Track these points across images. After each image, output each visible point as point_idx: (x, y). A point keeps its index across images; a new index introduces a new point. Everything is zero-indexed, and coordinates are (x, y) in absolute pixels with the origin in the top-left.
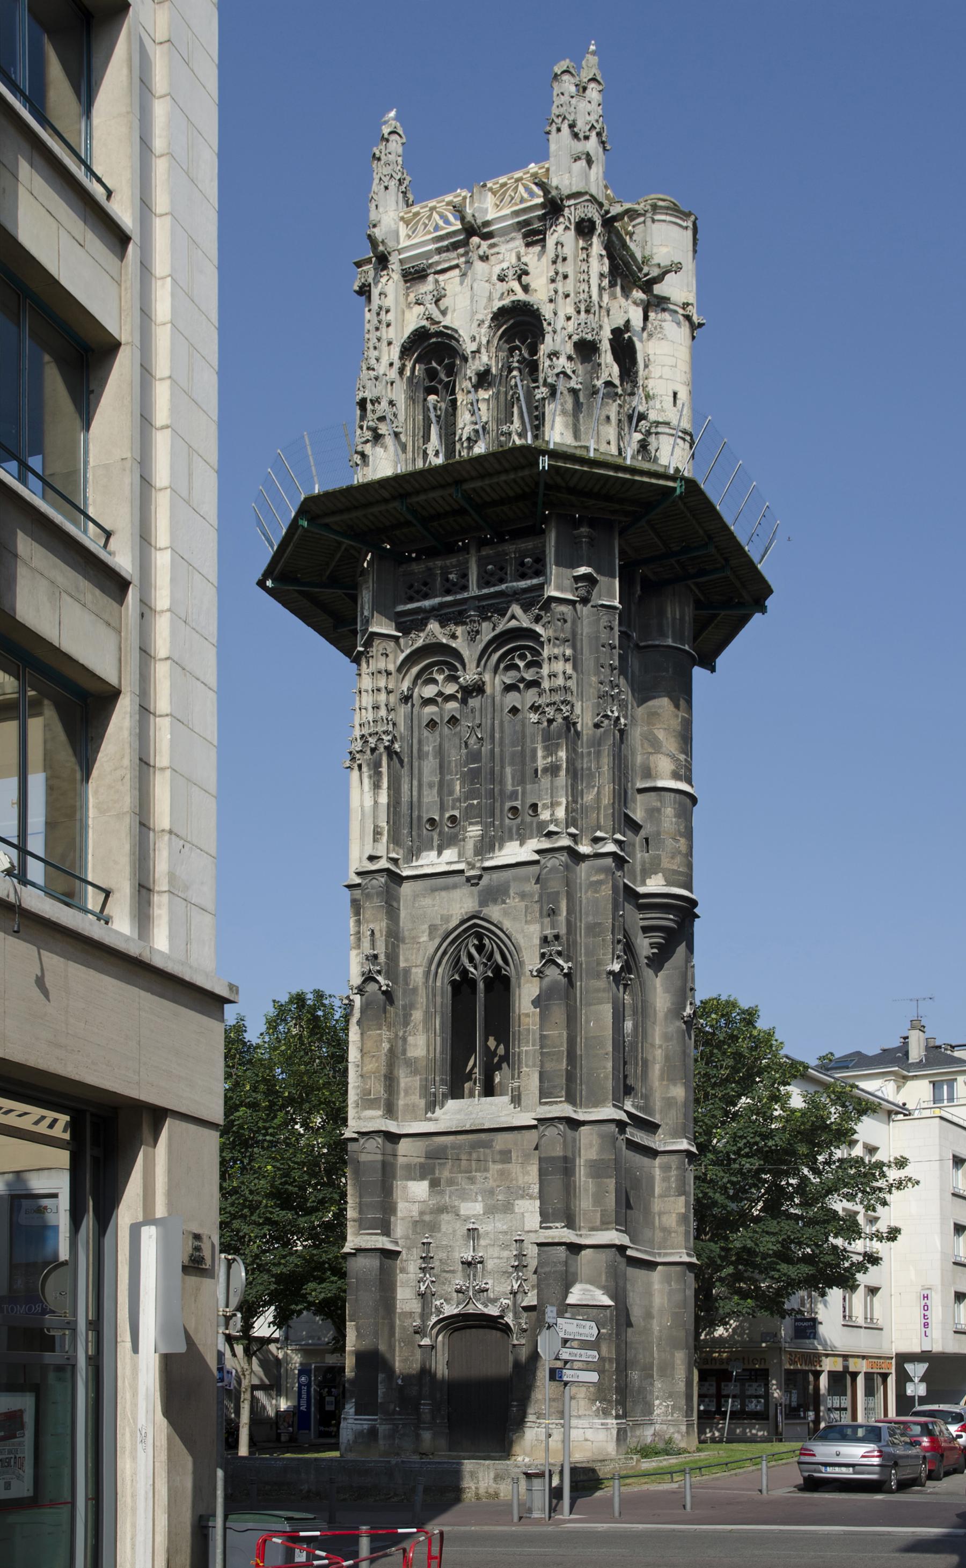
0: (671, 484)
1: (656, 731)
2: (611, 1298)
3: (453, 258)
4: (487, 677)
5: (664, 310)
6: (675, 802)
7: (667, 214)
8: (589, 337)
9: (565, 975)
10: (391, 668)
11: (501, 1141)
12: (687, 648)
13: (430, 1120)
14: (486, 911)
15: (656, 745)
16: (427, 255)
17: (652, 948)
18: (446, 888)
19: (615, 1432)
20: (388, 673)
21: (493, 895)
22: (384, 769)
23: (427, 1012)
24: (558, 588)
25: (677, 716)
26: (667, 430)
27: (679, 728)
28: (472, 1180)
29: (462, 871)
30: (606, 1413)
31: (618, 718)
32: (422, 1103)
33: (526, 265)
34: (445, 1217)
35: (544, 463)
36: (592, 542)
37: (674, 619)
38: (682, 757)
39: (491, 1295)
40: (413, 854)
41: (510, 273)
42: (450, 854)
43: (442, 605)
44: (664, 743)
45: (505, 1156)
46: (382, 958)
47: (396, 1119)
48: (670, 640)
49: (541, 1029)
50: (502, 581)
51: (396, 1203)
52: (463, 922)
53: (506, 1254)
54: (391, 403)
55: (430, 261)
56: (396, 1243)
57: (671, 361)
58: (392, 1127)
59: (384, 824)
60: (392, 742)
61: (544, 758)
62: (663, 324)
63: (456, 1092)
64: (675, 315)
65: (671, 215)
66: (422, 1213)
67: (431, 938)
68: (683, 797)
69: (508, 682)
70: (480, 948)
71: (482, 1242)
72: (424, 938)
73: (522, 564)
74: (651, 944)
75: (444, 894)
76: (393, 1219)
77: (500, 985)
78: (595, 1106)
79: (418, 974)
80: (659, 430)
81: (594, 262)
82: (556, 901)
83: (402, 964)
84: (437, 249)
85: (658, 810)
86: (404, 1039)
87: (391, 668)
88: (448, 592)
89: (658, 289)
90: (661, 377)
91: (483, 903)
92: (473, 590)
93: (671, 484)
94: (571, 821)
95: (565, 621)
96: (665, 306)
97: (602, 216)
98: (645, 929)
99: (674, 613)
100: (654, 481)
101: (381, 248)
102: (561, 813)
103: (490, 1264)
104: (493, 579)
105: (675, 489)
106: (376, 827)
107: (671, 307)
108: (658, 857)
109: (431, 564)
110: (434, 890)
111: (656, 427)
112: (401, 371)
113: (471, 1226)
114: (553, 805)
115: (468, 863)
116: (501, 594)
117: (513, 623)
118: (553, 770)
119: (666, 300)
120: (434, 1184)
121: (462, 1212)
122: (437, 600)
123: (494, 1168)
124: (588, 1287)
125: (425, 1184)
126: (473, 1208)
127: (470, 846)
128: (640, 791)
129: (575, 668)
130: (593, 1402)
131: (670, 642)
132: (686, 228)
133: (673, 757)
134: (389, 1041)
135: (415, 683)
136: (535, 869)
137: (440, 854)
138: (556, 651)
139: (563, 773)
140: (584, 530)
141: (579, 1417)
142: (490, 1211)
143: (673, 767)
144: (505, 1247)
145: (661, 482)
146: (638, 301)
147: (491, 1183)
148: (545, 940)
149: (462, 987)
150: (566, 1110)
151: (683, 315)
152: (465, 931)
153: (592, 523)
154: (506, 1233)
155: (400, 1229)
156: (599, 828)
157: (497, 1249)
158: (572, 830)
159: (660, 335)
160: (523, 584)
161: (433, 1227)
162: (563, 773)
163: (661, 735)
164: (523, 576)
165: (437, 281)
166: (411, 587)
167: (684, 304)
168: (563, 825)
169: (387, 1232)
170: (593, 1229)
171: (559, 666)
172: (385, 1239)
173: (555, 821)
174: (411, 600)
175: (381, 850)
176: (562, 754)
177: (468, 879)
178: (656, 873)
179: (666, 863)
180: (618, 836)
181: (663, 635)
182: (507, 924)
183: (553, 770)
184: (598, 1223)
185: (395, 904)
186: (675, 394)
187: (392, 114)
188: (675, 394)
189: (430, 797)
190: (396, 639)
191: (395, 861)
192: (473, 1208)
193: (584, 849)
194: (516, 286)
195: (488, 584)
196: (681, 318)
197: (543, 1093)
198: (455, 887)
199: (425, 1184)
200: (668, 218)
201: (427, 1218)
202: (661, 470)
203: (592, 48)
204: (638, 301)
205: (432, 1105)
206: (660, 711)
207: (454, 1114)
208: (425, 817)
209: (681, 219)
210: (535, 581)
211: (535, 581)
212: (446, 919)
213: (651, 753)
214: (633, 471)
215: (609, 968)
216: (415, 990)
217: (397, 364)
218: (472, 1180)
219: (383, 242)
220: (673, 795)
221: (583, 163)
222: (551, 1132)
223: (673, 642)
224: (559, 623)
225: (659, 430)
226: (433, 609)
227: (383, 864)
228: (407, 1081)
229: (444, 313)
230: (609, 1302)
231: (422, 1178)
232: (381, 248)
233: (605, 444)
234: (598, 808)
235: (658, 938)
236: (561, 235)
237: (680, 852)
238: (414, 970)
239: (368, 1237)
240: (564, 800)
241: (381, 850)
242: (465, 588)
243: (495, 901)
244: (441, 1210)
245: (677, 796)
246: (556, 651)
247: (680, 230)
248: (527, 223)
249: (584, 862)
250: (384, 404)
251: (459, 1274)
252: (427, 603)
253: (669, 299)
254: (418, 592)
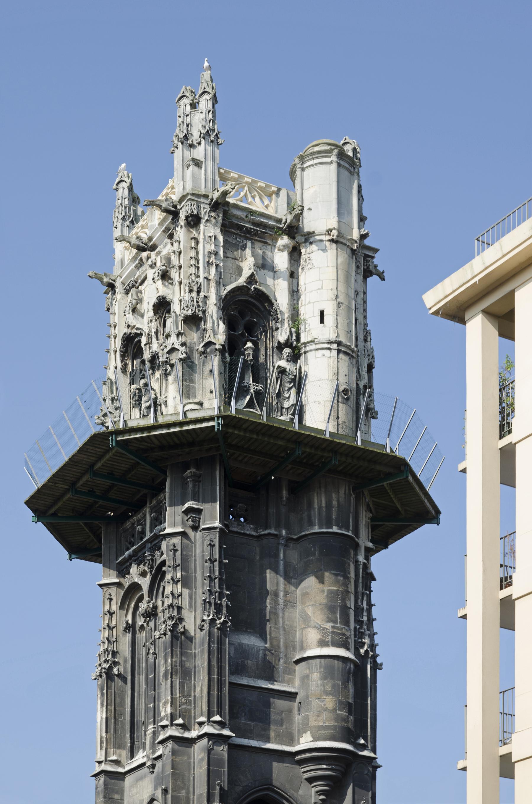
0: (211, 424)
1: (306, 609)
5: (311, 243)
6: (320, 667)
7: (313, 158)
8: (189, 313)
15: (306, 620)
16: (132, 273)
17: (320, 795)
25: (323, 591)
26: (314, 347)
27: (325, 601)
33: (114, 281)
36: (197, 479)
37: (320, 508)
44: (312, 618)
48: (317, 527)
55: (136, 277)
62: (311, 255)
64: (322, 243)
65: (317, 158)
68: (328, 660)
74: (317, 792)
80: (308, 349)
84: (136, 267)
90: (309, 302)
93: (211, 424)
95: (176, 551)
96: (311, 240)
97: (209, 204)
98: (310, 780)
99: (320, 502)
100: (198, 426)
101: (105, 280)
105: (214, 426)
107: (318, 238)
108: (307, 718)
111: (305, 347)
119: (311, 234)
128: (298, 662)
129: (184, 586)
132: (331, 162)
133: (320, 628)
143: (319, 637)
145: (205, 425)
146: (282, 248)
151: (329, 240)
153: (198, 464)
159: (310, 266)
163: (309, 611)
167: (327, 231)
178: (305, 732)
179: (313, 722)
181: (311, 524)
186: (322, 313)
187: (123, 165)
188: (322, 313)
196: (328, 244)
198: (141, 778)
200: (316, 161)
203: (206, 64)
204: (282, 248)
206: (309, 591)
209: (326, 157)
213: (303, 628)
217: (119, 365)
219: (105, 275)
220: (318, 661)
224: (172, 553)
225: (308, 349)
226: (130, 556)
232: (105, 280)
233: (209, 393)
235: (321, 786)
237: (325, 710)
245: (323, 661)
247: (327, 166)
249: (195, 744)
253: (314, 233)
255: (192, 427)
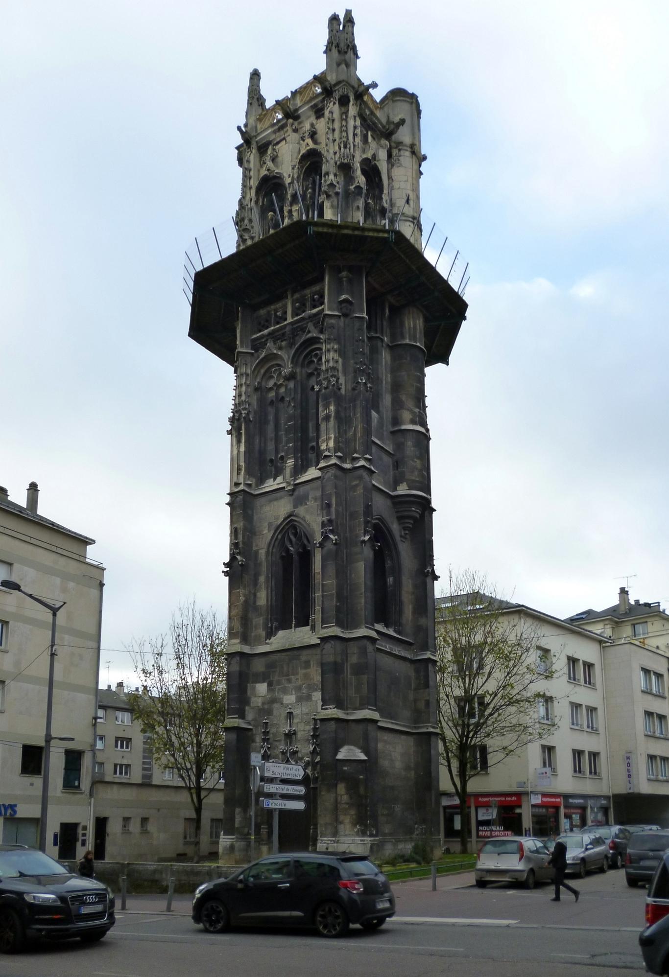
2: (366, 755)
3: (281, 135)
4: (298, 370)
9: (335, 544)
10: (249, 371)
11: (304, 655)
12: (418, 344)
13: (268, 644)
14: (297, 511)
18: (276, 499)
19: (369, 846)
20: (247, 375)
21: (300, 501)
22: (243, 431)
23: (267, 577)
24: (329, 309)
28: (289, 681)
29: (284, 488)
30: (364, 833)
31: (365, 384)
32: (263, 634)
34: (276, 706)
35: (311, 230)
36: (350, 281)
37: (410, 328)
38: (417, 410)
39: (300, 755)
40: (261, 481)
41: (307, 134)
42: (280, 479)
43: (274, 331)
45: (307, 665)
46: (241, 545)
47: (250, 645)
49: (323, 580)
50: (304, 312)
51: (249, 698)
52: (285, 519)
53: (308, 728)
54: (250, 221)
56: (249, 724)
57: (405, 178)
58: (246, 649)
59: (242, 464)
60: (248, 414)
61: (323, 411)
63: (285, 625)
66: (263, 703)
67: (269, 531)
69: (309, 371)
70: (295, 535)
71: (295, 721)
72: (266, 531)
73: (314, 300)
75: (275, 503)
76: (247, 708)
77: (306, 557)
78: (356, 628)
79: (262, 553)
81: (351, 123)
82: (330, 499)
83: (254, 549)
85: (403, 444)
86: (255, 595)
87: (249, 371)
88: (278, 323)
89: (394, 137)
91: (295, 506)
92: (290, 320)
94: (337, 449)
102: (331, 444)
103: (300, 735)
104: (299, 312)
106: (239, 466)
109: (268, 309)
110: (271, 501)
112: (257, 202)
113: (289, 710)
114: (328, 439)
115: (287, 482)
116: (303, 319)
117: (310, 335)
118: (327, 418)
120: (270, 685)
121: (284, 702)
122: (272, 328)
123: (302, 672)
124: (352, 747)
125: (265, 685)
126: (290, 699)
127: (288, 472)
130: (355, 825)
131: (407, 341)
134: (245, 595)
135: (262, 379)
136: (319, 483)
137: (275, 480)
138: (328, 346)
139: (332, 419)
140: (344, 274)
141: (346, 835)
142: (299, 699)
144: (308, 723)
147: (300, 682)
148: (323, 525)
149: (287, 559)
150: (336, 631)
152: (287, 524)
153: (350, 269)
154: (307, 714)
155: (250, 715)
156: (356, 452)
157: (303, 724)
158: (339, 454)
160: (314, 311)
161: (269, 712)
162: (332, 419)
164: (315, 307)
165: (274, 149)
166: (260, 323)
168: (332, 451)
169: (242, 716)
170: (356, 709)
171: (331, 355)
172: (240, 720)
173: (328, 449)
174: (260, 331)
175: (241, 480)
176: (332, 408)
177: (288, 491)
180: (368, 456)
182: (308, 518)
183: (327, 418)
184: (358, 705)
185: (250, 512)
189: (271, 446)
190: (252, 354)
191: (249, 485)
192: (290, 699)
193: (347, 466)
194: (309, 141)
195: (297, 315)
197: (324, 622)
198: (281, 498)
199: (265, 685)
201: (266, 707)
202: (379, 227)
205: (270, 634)
207: (282, 639)
208: (268, 458)
210: (320, 308)
211: (320, 308)
212: (277, 518)
214: (363, 229)
215: (362, 538)
216: (260, 564)
217: (254, 199)
218: (289, 681)
221: (343, 66)
222: (328, 646)
223: (410, 340)
226: (269, 334)
227: (242, 487)
228: (258, 621)
229: (277, 166)
230: (363, 757)
231: (264, 682)
234: (355, 440)
236: (333, 108)
238: (260, 551)
239: (231, 720)
240: (333, 436)
241: (241, 480)
242: (286, 319)
243: (301, 504)
244: (273, 701)
246: (328, 346)
248: (315, 105)
250: (246, 221)
251: (283, 742)
252: (266, 332)
254: (263, 326)
255: (371, 234)
